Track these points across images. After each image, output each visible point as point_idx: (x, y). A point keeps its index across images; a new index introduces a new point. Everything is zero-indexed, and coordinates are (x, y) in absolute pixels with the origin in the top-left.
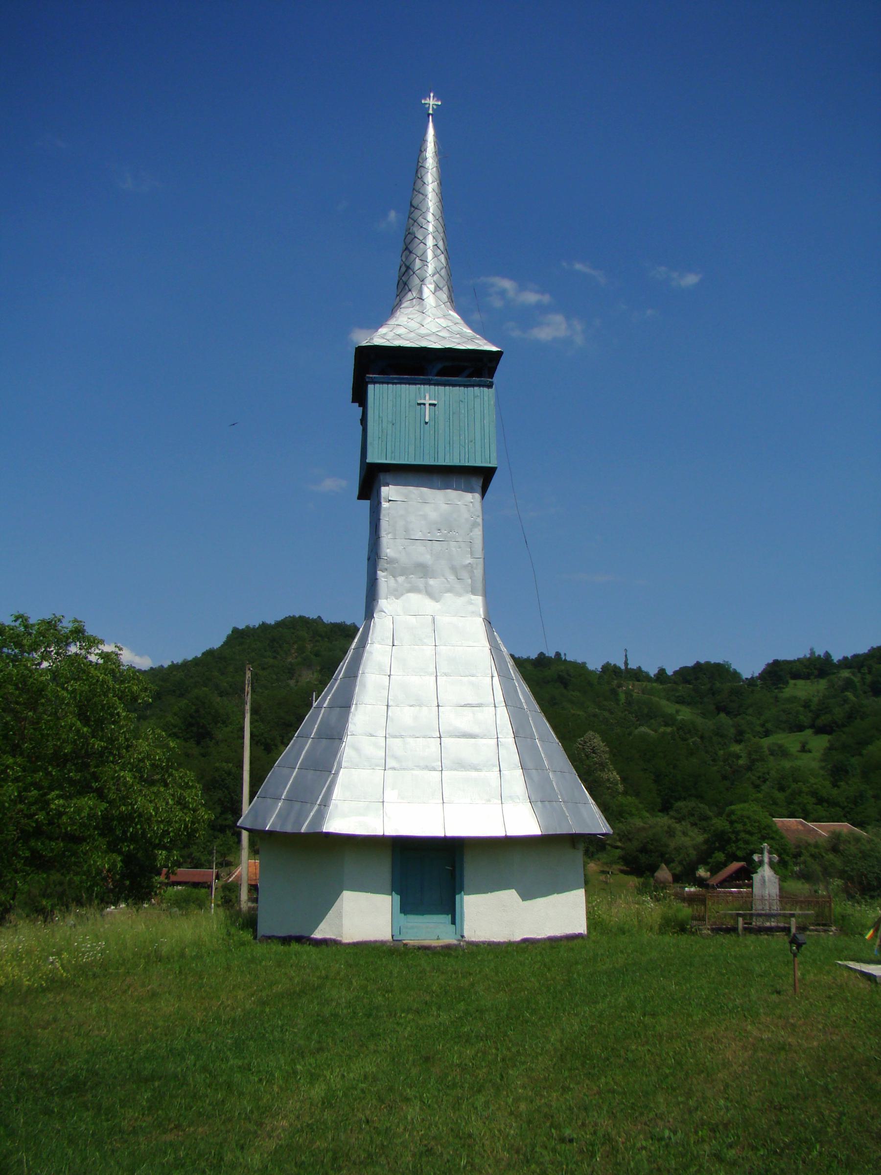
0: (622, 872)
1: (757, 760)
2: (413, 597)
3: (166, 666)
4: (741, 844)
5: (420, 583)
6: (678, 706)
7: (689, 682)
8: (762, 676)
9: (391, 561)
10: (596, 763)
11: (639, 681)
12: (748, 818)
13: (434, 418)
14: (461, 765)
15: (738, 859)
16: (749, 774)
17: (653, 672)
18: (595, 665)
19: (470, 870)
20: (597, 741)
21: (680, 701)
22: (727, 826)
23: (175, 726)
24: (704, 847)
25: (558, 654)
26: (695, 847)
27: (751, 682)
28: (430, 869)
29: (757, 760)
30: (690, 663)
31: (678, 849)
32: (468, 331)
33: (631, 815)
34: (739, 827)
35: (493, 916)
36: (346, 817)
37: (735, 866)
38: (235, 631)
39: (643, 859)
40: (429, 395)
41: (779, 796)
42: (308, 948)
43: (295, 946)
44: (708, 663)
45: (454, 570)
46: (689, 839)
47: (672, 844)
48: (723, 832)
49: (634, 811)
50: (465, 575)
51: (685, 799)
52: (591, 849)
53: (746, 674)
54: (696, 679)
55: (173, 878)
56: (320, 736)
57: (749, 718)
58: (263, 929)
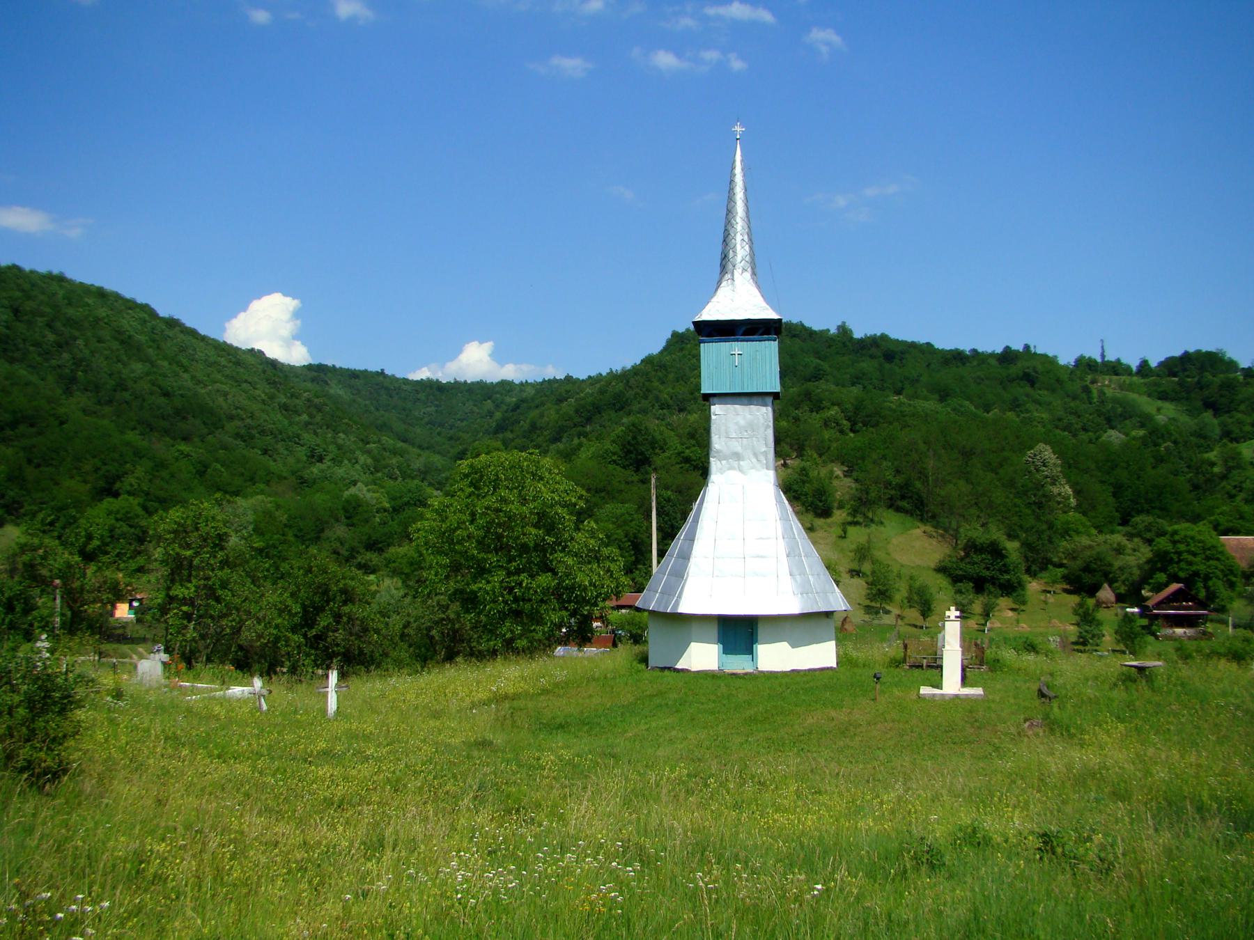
0: (1066, 591)
1: (1233, 468)
2: (731, 473)
3: (604, 374)
4: (1183, 565)
5: (735, 464)
6: (1160, 403)
9: (718, 452)
10: (1047, 477)
11: (1117, 374)
12: (1192, 538)
13: (741, 363)
15: (1178, 580)
16: (1224, 483)
17: (1134, 365)
18: (1066, 358)
19: (761, 631)
20: (1048, 453)
21: (1163, 397)
22: (1170, 547)
23: (614, 454)
24: (1146, 567)
25: (1027, 347)
26: (1139, 567)
28: (739, 632)
29: (1233, 468)
30: (1177, 353)
32: (764, 304)
33: (1078, 533)
34: (1182, 547)
35: (774, 656)
38: (675, 334)
39: (1087, 579)
42: (673, 674)
43: (667, 673)
44: (1198, 352)
45: (755, 455)
46: (1136, 556)
48: (1166, 553)
49: (1081, 529)
51: (1148, 512)
54: (1185, 370)
55: (620, 603)
57: (1239, 415)
58: (652, 663)
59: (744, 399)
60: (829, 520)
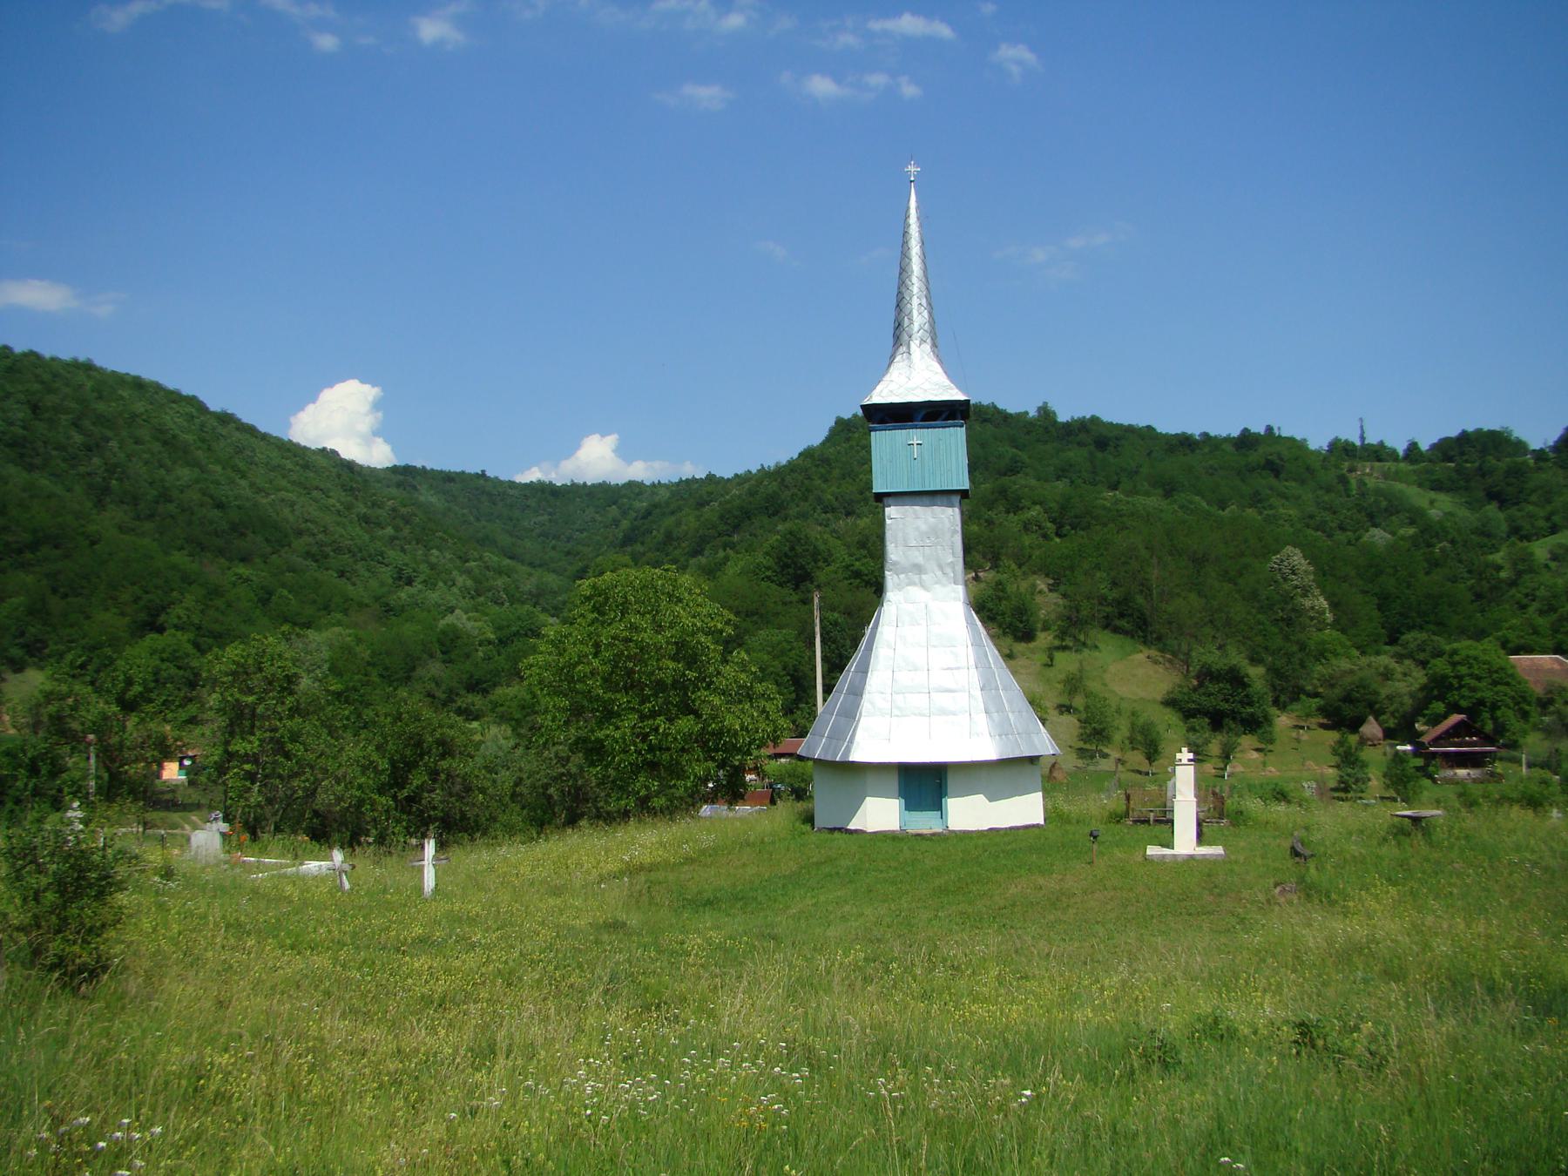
0: (1323, 726)
3: (754, 471)
4: (1465, 692)
5: (916, 578)
6: (1433, 495)
7: (1450, 460)
8: (1556, 448)
9: (895, 564)
10: (1296, 587)
11: (1379, 460)
12: (1476, 659)
13: (921, 454)
14: (943, 712)
15: (1459, 710)
17: (1401, 448)
18: (1318, 442)
19: (952, 781)
20: (1297, 558)
21: (1437, 486)
23: (768, 568)
24: (1420, 695)
25: (1269, 429)
26: (1412, 695)
27: (1540, 455)
28: (924, 783)
30: (1453, 432)
31: (1390, 698)
32: (947, 382)
33: (1336, 655)
34: (1463, 670)
35: (967, 813)
36: (862, 752)
37: (1455, 718)
39: (1348, 711)
40: (916, 437)
41: (1542, 622)
42: (845, 836)
43: (837, 835)
44: (1479, 432)
45: (941, 567)
46: (1407, 682)
47: (1384, 692)
48: (1445, 677)
49: (1340, 650)
50: (949, 570)
52: (1283, 698)
53: (1535, 444)
54: (1462, 454)
56: (849, 692)
57: (1531, 508)
58: (818, 823)
59: (926, 499)
60: (1032, 645)
